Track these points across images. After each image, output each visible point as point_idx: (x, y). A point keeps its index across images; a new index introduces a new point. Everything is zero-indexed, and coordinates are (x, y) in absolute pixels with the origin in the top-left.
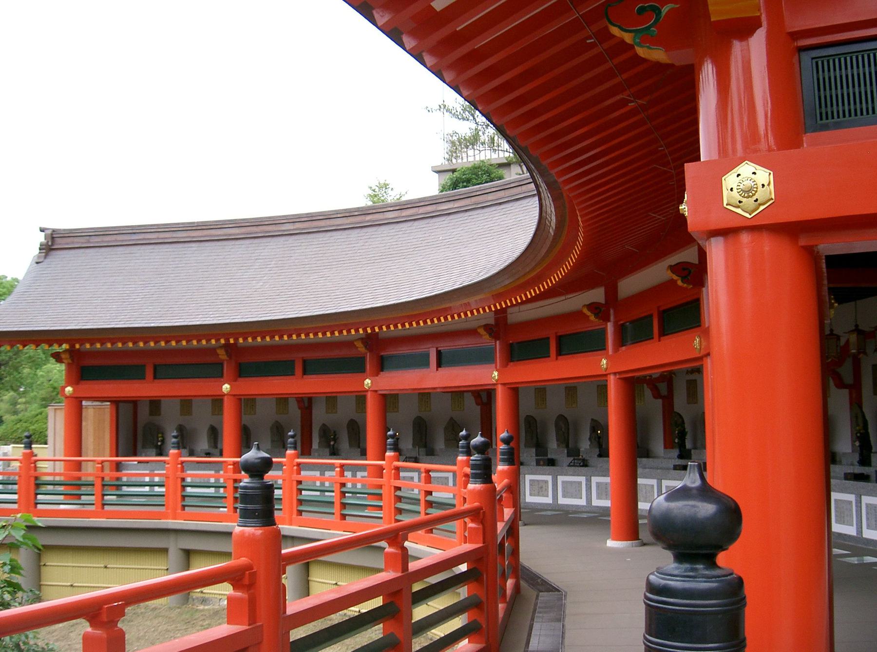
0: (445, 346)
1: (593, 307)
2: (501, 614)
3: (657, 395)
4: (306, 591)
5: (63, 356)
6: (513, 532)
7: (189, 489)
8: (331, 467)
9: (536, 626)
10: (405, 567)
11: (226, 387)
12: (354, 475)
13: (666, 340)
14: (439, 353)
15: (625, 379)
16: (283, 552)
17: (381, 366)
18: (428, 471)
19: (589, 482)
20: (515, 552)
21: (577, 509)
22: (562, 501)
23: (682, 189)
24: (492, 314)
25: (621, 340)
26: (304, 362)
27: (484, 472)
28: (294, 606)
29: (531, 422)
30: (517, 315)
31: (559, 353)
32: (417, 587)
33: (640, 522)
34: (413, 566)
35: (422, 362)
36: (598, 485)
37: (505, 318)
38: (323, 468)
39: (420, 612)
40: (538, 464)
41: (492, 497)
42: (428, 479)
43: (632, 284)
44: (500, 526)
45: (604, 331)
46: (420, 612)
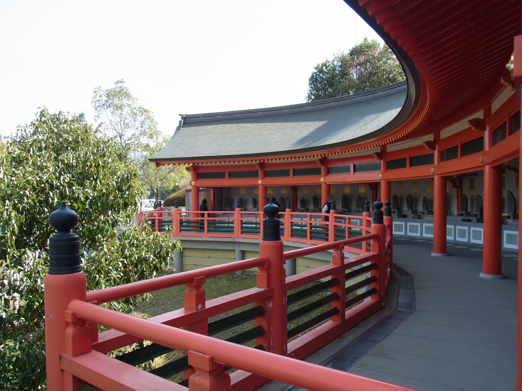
0: (357, 163)
1: (428, 143)
2: (386, 284)
3: (455, 186)
4: (294, 272)
5: (190, 168)
6: (390, 246)
7: (244, 225)
8: (306, 216)
9: (401, 291)
10: (342, 262)
11: (260, 182)
12: (316, 220)
13: (465, 158)
14: (354, 166)
15: (442, 177)
16: (284, 253)
17: (328, 172)
18: (349, 219)
19: (422, 225)
20: (391, 256)
21: (415, 238)
22: (409, 234)
23: (512, 50)
24: (380, 147)
25: (441, 158)
26: (294, 170)
27: (379, 219)
28: (289, 279)
29: (395, 198)
30: (390, 148)
31: (411, 165)
32: (347, 271)
33: (447, 245)
34: (346, 261)
35: (347, 170)
36: (426, 227)
37: (386, 149)
38: (302, 217)
39: (349, 284)
40: (398, 216)
41: (383, 230)
42: (350, 223)
43: (446, 133)
44: (386, 244)
45: (433, 155)
46: (349, 284)
